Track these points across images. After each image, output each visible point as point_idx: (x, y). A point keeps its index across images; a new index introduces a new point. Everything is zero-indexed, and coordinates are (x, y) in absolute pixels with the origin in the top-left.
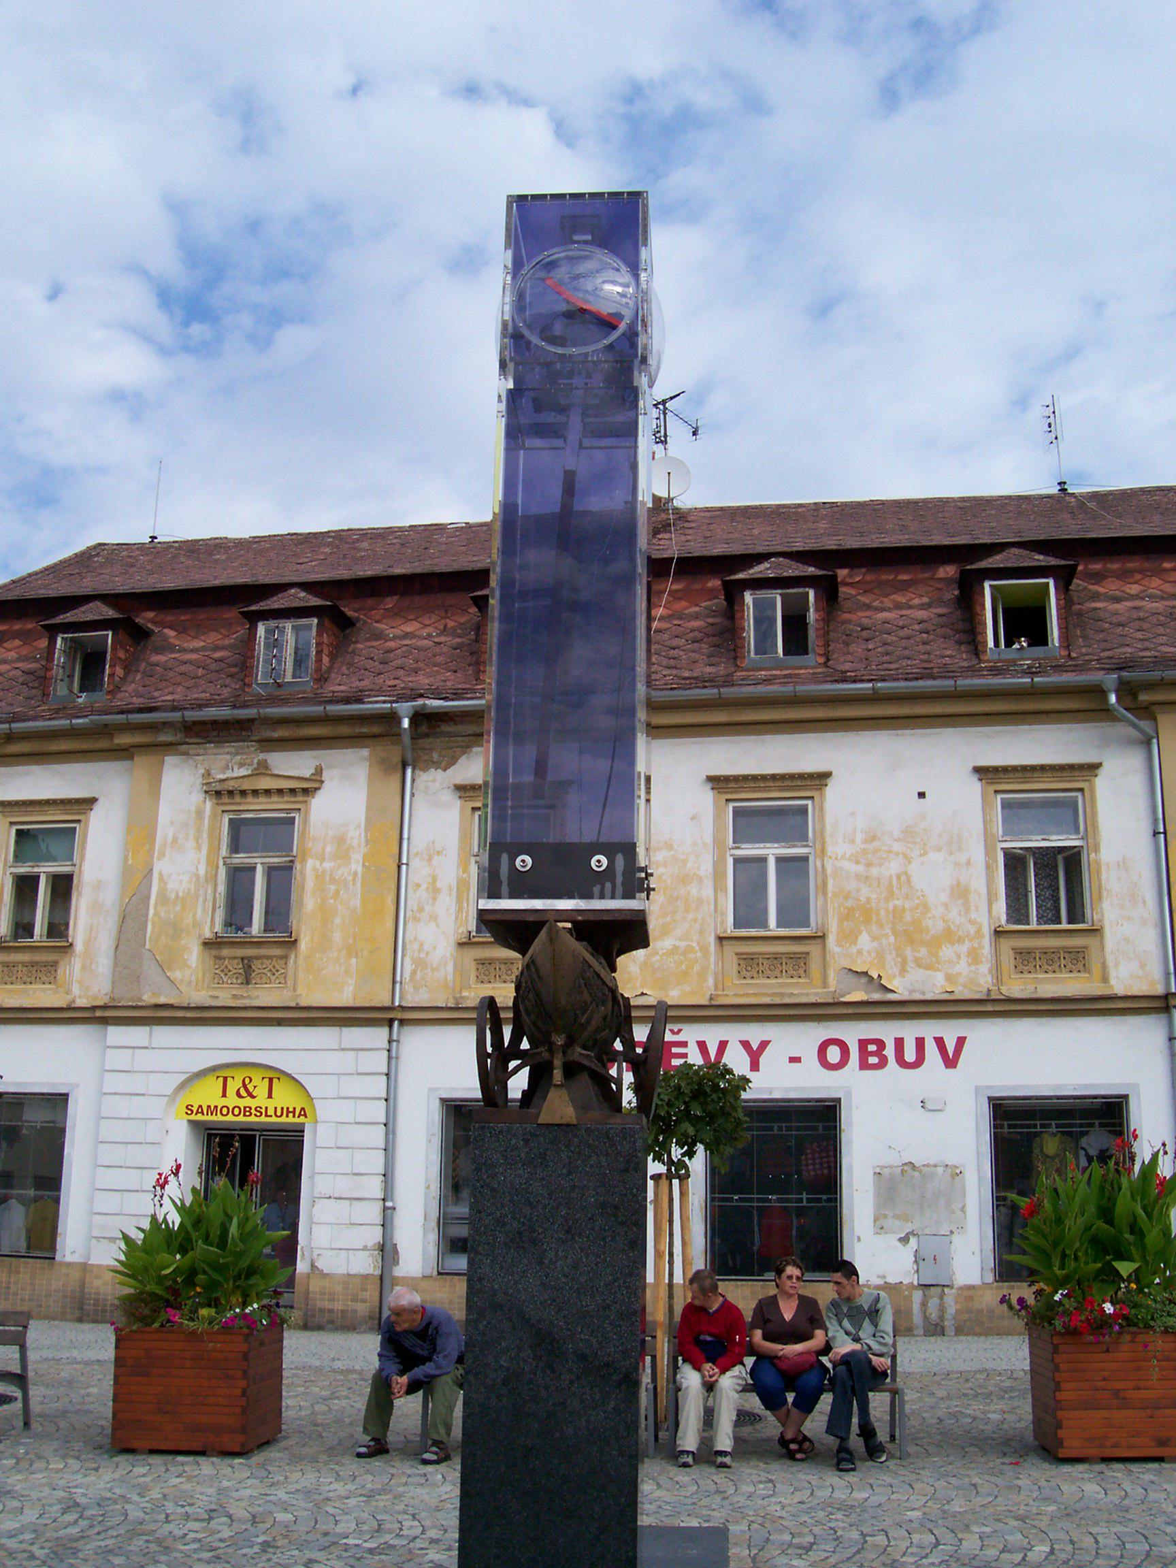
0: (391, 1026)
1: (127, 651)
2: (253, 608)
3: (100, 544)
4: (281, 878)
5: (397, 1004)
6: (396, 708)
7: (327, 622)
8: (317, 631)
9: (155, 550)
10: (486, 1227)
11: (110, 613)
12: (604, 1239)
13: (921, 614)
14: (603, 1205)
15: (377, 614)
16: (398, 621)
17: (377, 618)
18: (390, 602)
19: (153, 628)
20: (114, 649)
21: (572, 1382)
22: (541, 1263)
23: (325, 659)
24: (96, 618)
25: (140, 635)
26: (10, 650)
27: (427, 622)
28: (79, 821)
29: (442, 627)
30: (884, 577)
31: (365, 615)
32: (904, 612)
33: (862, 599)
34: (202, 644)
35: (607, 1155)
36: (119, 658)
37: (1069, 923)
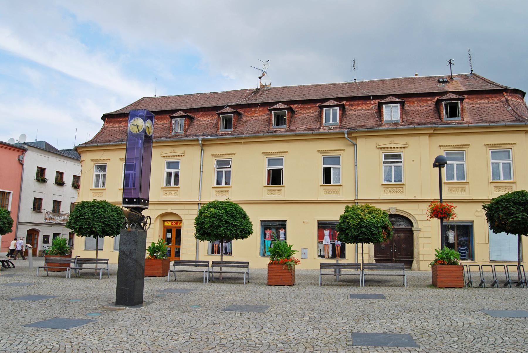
0: (198, 205)
2: (271, 108)
4: (228, 174)
7: (187, 119)
11: (232, 110)
13: (312, 115)
18: (201, 113)
23: (187, 127)
25: (239, 114)
27: (209, 118)
30: (305, 106)
32: (309, 114)
33: (300, 111)
37: (217, 185)
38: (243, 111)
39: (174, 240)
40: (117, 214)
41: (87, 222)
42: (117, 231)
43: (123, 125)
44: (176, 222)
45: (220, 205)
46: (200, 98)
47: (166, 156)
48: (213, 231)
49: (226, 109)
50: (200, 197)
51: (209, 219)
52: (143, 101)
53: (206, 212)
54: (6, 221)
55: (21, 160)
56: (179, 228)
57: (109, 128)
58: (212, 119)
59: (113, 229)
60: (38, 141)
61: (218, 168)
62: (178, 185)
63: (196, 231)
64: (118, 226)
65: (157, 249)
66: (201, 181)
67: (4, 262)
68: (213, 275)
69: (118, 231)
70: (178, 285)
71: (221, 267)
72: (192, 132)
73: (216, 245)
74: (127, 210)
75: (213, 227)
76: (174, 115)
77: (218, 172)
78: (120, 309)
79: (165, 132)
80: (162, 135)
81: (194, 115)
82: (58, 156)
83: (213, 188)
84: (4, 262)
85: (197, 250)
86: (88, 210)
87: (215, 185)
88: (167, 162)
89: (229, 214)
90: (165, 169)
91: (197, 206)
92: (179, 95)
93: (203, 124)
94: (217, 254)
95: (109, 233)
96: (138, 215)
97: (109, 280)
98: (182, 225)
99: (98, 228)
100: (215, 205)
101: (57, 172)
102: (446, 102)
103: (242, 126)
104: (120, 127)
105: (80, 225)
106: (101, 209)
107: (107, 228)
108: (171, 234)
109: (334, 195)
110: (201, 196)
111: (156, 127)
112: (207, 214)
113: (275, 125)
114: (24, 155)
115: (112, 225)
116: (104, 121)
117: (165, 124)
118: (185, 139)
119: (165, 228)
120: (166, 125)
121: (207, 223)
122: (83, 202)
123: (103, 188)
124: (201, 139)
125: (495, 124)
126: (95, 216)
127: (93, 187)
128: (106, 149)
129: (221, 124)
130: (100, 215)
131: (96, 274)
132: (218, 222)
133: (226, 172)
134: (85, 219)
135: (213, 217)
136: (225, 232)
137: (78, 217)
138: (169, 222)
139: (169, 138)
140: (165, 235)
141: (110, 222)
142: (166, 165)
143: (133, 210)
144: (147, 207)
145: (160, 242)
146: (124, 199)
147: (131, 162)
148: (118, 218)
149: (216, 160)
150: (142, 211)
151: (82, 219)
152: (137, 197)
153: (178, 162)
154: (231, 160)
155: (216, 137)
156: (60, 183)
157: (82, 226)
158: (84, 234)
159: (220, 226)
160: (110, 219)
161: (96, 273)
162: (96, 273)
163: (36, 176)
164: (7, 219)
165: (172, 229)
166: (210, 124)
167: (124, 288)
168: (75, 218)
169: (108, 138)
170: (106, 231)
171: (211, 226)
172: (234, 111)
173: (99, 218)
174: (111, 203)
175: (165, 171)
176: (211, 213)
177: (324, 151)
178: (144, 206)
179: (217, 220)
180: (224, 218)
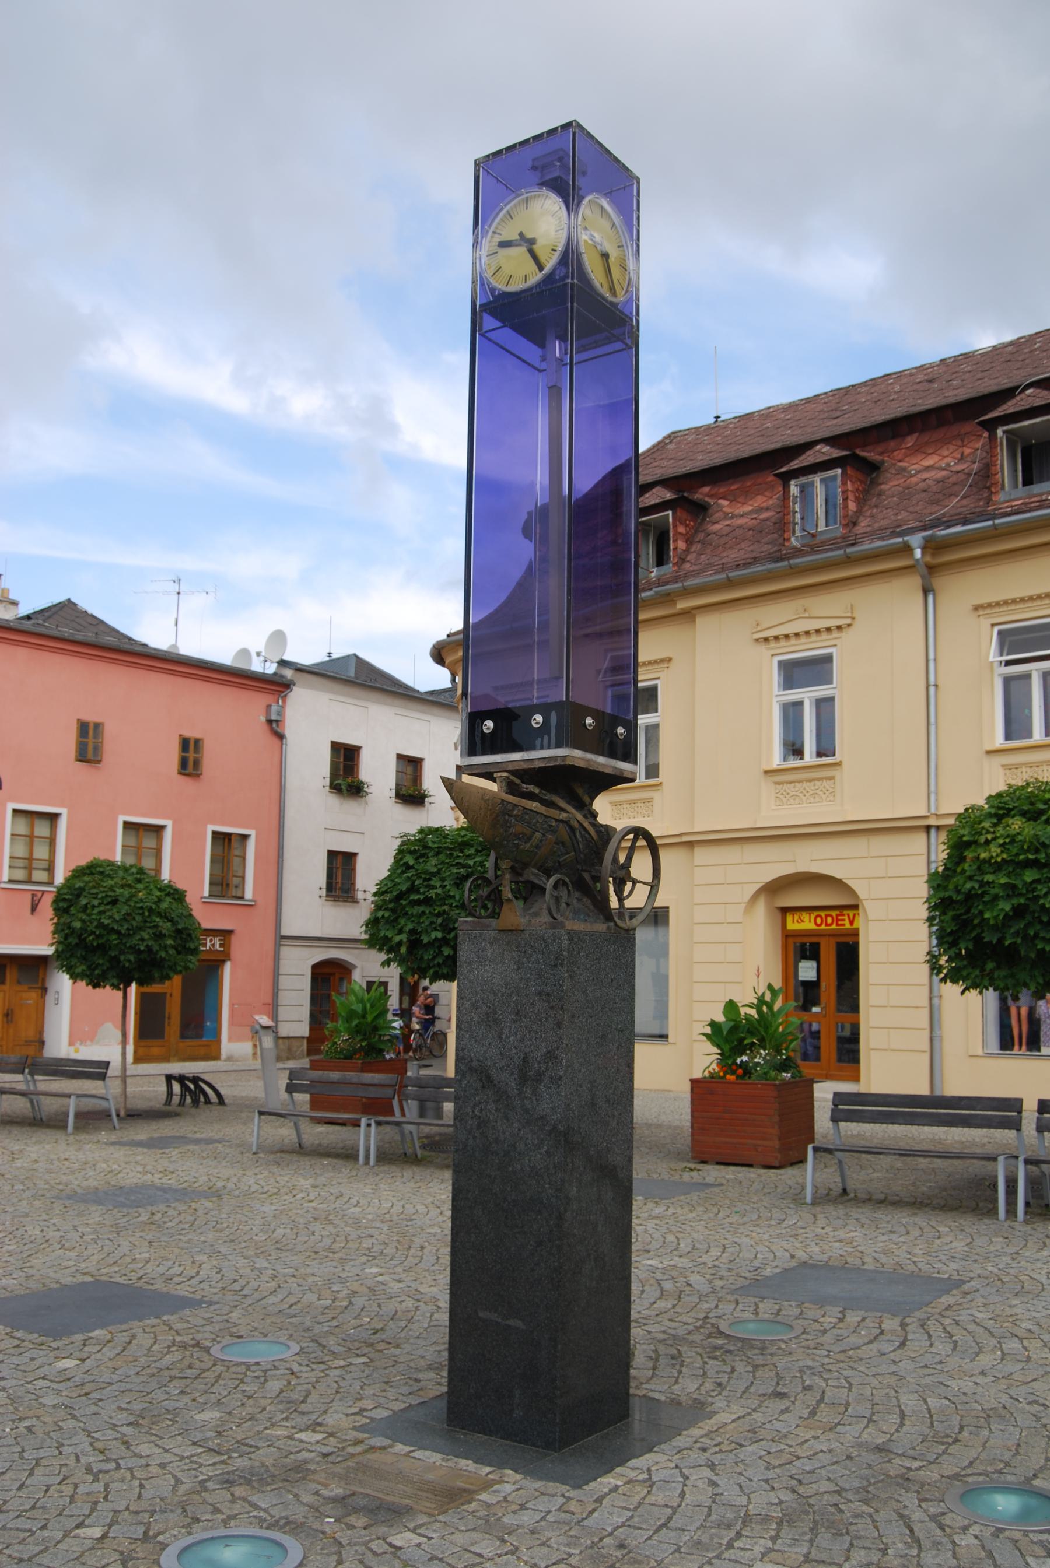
1: (687, 526)
3: (673, 433)
5: (933, 810)
7: (849, 471)
9: (718, 427)
12: (540, 1020)
14: (540, 994)
16: (920, 456)
17: (900, 457)
18: (910, 441)
20: (675, 526)
22: (500, 1038)
23: (852, 506)
24: (657, 501)
27: (946, 453)
28: (658, 678)
29: (959, 456)
34: (750, 508)
35: (543, 953)
36: (681, 534)
37: (647, 778)
39: (829, 988)
41: (439, 915)
44: (834, 913)
46: (897, 388)
47: (776, 638)
48: (1027, 939)
49: (1023, 396)
51: (1008, 875)
53: (987, 842)
54: (166, 927)
55: (277, 721)
56: (850, 940)
58: (962, 458)
60: (334, 656)
61: (1008, 663)
65: (751, 1032)
66: (932, 729)
67: (187, 1082)
70: (857, 1234)
73: (1019, 1008)
74: (492, 786)
75: (1029, 918)
77: (1008, 681)
79: (766, 540)
80: (754, 555)
81: (881, 454)
82: (398, 702)
83: (988, 752)
84: (187, 1082)
85: (937, 1032)
88: (780, 662)
90: (776, 691)
91: (922, 837)
92: (810, 394)
93: (922, 485)
94: (1029, 1049)
98: (859, 923)
100: (1032, 804)
101: (400, 757)
105: (413, 932)
108: (814, 964)
110: (937, 794)
111: (728, 529)
112: (995, 850)
113: (1016, 486)
114: (284, 702)
117: (760, 510)
119: (791, 940)
120: (765, 515)
129: (1006, 469)
134: (427, 901)
137: (400, 896)
138: (805, 916)
139: (781, 559)
140: (789, 971)
142: (775, 676)
145: (761, 1001)
149: (996, 630)
150: (593, 799)
151: (419, 903)
153: (828, 659)
155: (990, 523)
156: (410, 796)
158: (430, 968)
163: (328, 775)
164: (171, 920)
165: (818, 944)
166: (953, 479)
167: (494, 1316)
168: (391, 901)
171: (1019, 912)
175: (775, 700)
176: (1013, 841)
177: (998, 604)
178: (602, 762)
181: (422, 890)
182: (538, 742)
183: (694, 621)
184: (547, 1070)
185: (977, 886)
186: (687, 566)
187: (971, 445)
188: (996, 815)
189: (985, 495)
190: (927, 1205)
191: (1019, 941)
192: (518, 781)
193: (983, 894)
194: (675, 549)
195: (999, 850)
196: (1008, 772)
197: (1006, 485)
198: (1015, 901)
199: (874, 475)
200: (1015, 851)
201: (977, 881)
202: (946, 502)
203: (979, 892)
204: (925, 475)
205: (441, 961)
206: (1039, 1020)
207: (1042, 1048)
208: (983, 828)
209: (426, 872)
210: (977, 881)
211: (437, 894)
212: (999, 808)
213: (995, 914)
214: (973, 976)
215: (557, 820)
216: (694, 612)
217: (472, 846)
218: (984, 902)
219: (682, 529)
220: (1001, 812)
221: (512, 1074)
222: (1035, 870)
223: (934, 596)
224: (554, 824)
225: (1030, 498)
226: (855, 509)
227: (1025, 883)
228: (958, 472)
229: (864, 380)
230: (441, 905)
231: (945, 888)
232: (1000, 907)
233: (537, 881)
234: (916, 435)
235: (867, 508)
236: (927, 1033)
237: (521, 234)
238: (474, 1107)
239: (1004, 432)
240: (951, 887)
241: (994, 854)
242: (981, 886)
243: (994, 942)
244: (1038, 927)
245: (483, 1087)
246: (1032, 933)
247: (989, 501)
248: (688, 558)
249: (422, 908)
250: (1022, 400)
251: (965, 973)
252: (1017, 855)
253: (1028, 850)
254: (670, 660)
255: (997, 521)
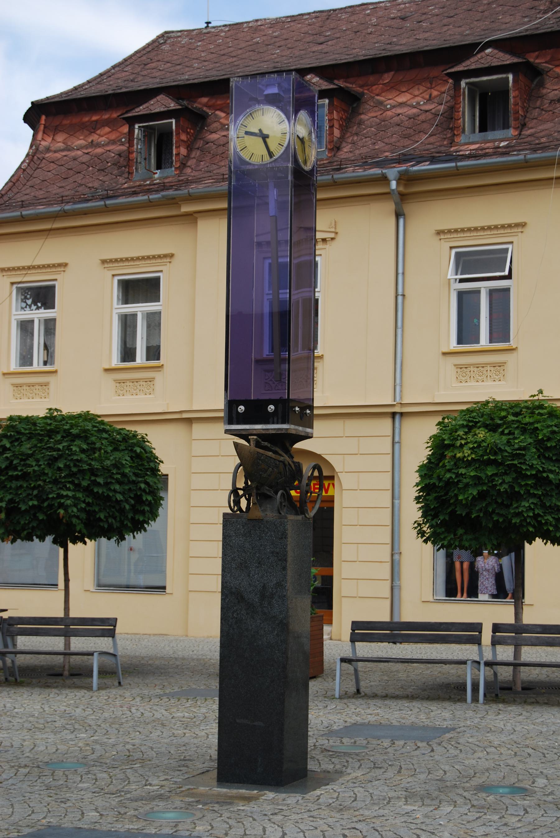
1: (188, 133)
3: (166, 33)
6: (385, 173)
8: (329, 110)
10: (228, 561)
11: (508, 59)
12: (273, 566)
14: (272, 553)
15: (376, 89)
16: (395, 93)
17: (377, 92)
18: (387, 78)
19: (208, 111)
20: (178, 134)
21: (260, 624)
22: (249, 576)
24: (162, 109)
26: (102, 136)
27: (417, 93)
28: (161, 271)
29: (428, 97)
31: (368, 90)
35: (274, 532)
36: (183, 141)
37: (148, 359)
38: (548, 58)
40: (132, 457)
41: (34, 488)
42: (133, 519)
43: (103, 140)
45: (511, 418)
46: (374, 20)
49: (482, 54)
50: (398, 388)
51: (476, 469)
52: (166, 47)
53: (462, 446)
57: (55, 152)
59: (122, 511)
61: (461, 281)
62: (158, 359)
63: (420, 514)
64: (138, 499)
66: (399, 331)
68: (495, 674)
69: (137, 517)
71: (517, 647)
72: (357, 152)
73: (462, 563)
75: (489, 500)
76: (142, 110)
77: (461, 295)
78: (248, 799)
81: (361, 87)
83: (444, 354)
85: (396, 583)
86: (35, 446)
87: (115, 361)
88: (119, 281)
89: (547, 449)
90: (115, 305)
91: (388, 422)
93: (396, 119)
94: (469, 596)
95: (110, 525)
96: (283, 462)
97: (120, 691)
99: (75, 510)
102: (141, 125)
103: (546, 116)
104: (92, 144)
105: (11, 501)
106: (77, 442)
107: (100, 511)
109: (142, 396)
110: (401, 386)
112: (467, 452)
113: (474, 131)
115: (119, 497)
116: (33, 126)
118: (338, 176)
121: (467, 485)
122: (11, 418)
123: (48, 368)
124: (398, 175)
125: (425, 166)
126: (59, 469)
127: (14, 366)
128: (50, 230)
130: (75, 466)
131: (66, 673)
132: (508, 479)
133: (492, 292)
134: (25, 476)
135: (490, 462)
136: (536, 516)
141: (110, 489)
143: (266, 444)
144: (309, 430)
146: (231, 404)
147: (25, 279)
148: (135, 474)
149: (454, 251)
151: (17, 478)
152: (276, 397)
154: (510, 247)
155: (453, 164)
157: (18, 503)
158: (24, 529)
159: (515, 496)
160: (111, 477)
161: (67, 667)
162: (67, 667)
166: (423, 117)
169: (54, 190)
170: (100, 519)
171: (482, 496)
172: (516, 60)
173: (73, 475)
174: (106, 420)
176: (479, 446)
177: (456, 231)
179: (506, 474)
180: (532, 467)
181: (19, 468)
182: (271, 420)
183: (196, 222)
184: (277, 592)
185: (454, 476)
186: (188, 171)
187: (438, 88)
188: (467, 426)
189: (449, 135)
190: (417, 698)
191: (482, 515)
192: (260, 440)
193: (459, 481)
194: (178, 155)
195: (469, 452)
196: (459, 370)
197: (466, 129)
198: (480, 488)
199: (355, 105)
200: (481, 453)
201: (454, 473)
202: (416, 138)
203: (456, 481)
204: (399, 111)
205: (35, 525)
206: (478, 572)
207: (479, 595)
208: (459, 435)
209: (22, 454)
210: (454, 473)
211: (34, 471)
212: (469, 421)
213: (466, 497)
214: (449, 538)
215: (279, 461)
216: (195, 215)
217: (58, 433)
218: (458, 488)
219: (184, 137)
220: (471, 424)
221: (256, 594)
222: (494, 466)
223: (404, 219)
224: (278, 463)
225: (486, 143)
226: (339, 136)
227: (487, 476)
228: (427, 111)
229: (343, 6)
230: (36, 481)
231: (430, 477)
232: (470, 492)
233: (269, 493)
234: (392, 73)
235: (349, 134)
236: (388, 583)
237: (260, 130)
238: (233, 613)
239: (467, 84)
240: (435, 476)
241: (466, 455)
242: (456, 477)
243: (463, 515)
244: (495, 506)
245: (239, 602)
246: (491, 510)
247: (452, 143)
248: (189, 164)
249: (19, 483)
250: (482, 58)
251: (442, 537)
252: (482, 456)
253: (490, 453)
254: (172, 256)
255: (459, 164)
